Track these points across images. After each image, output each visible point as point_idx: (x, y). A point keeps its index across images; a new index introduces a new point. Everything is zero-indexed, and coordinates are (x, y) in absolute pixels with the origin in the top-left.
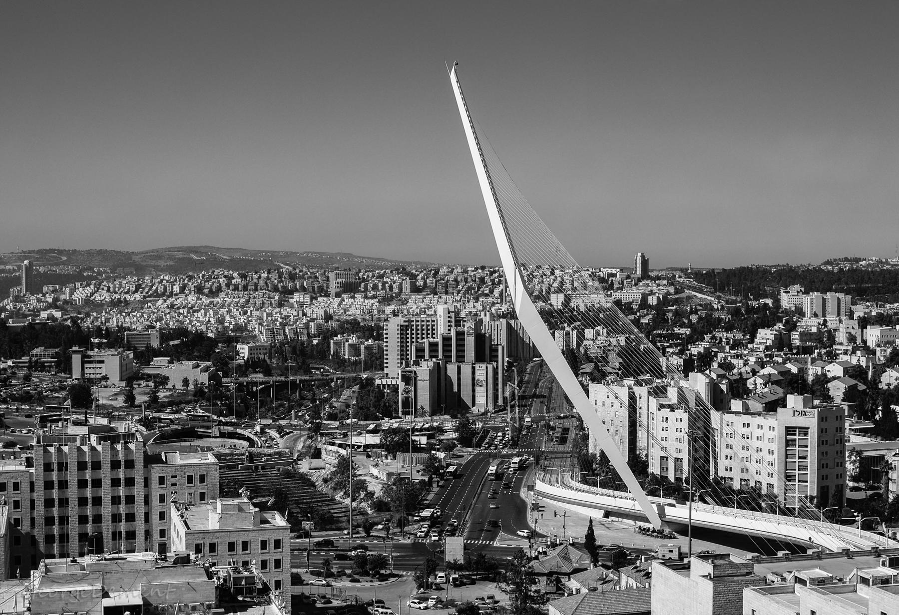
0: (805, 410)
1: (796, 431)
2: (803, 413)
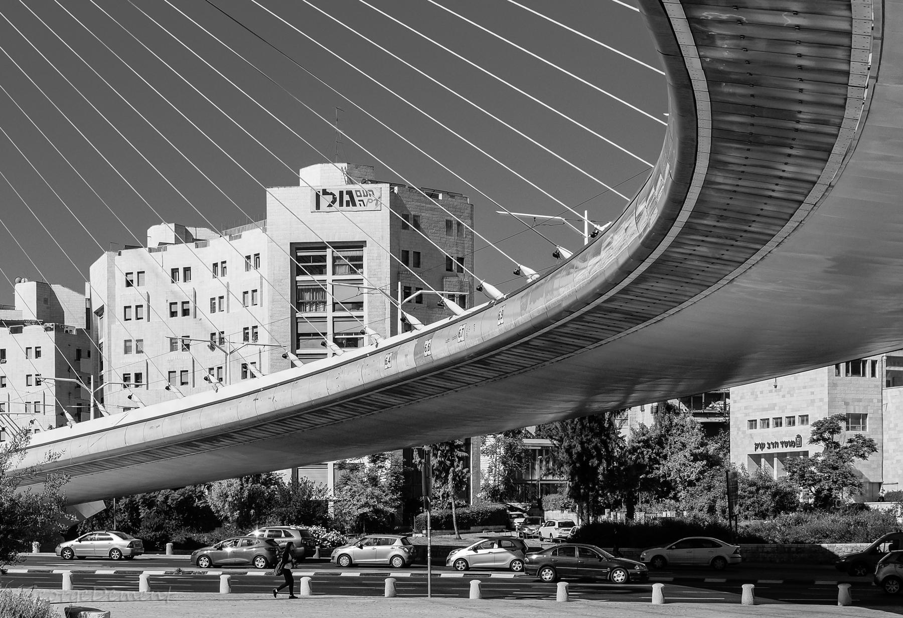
0: (351, 187)
1: (323, 259)
2: (346, 198)
